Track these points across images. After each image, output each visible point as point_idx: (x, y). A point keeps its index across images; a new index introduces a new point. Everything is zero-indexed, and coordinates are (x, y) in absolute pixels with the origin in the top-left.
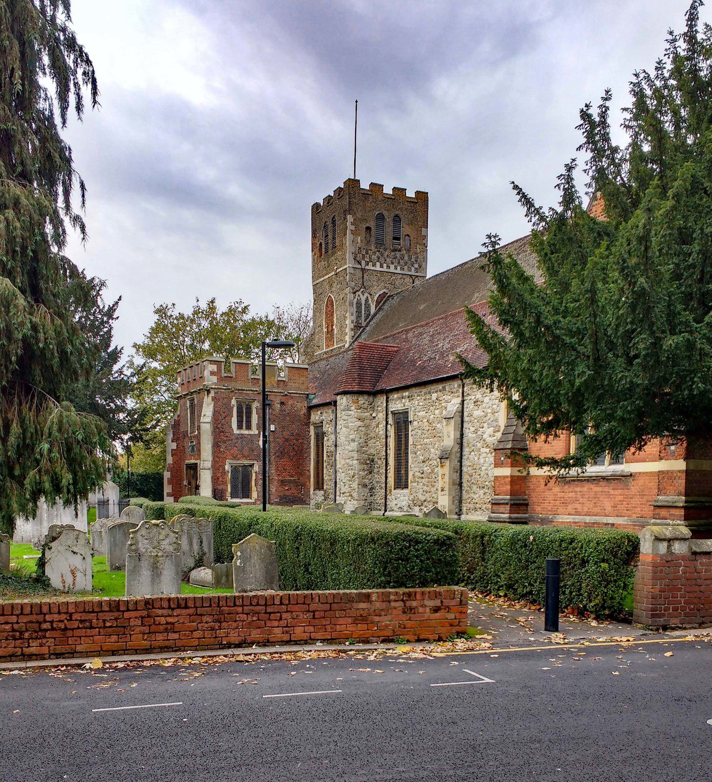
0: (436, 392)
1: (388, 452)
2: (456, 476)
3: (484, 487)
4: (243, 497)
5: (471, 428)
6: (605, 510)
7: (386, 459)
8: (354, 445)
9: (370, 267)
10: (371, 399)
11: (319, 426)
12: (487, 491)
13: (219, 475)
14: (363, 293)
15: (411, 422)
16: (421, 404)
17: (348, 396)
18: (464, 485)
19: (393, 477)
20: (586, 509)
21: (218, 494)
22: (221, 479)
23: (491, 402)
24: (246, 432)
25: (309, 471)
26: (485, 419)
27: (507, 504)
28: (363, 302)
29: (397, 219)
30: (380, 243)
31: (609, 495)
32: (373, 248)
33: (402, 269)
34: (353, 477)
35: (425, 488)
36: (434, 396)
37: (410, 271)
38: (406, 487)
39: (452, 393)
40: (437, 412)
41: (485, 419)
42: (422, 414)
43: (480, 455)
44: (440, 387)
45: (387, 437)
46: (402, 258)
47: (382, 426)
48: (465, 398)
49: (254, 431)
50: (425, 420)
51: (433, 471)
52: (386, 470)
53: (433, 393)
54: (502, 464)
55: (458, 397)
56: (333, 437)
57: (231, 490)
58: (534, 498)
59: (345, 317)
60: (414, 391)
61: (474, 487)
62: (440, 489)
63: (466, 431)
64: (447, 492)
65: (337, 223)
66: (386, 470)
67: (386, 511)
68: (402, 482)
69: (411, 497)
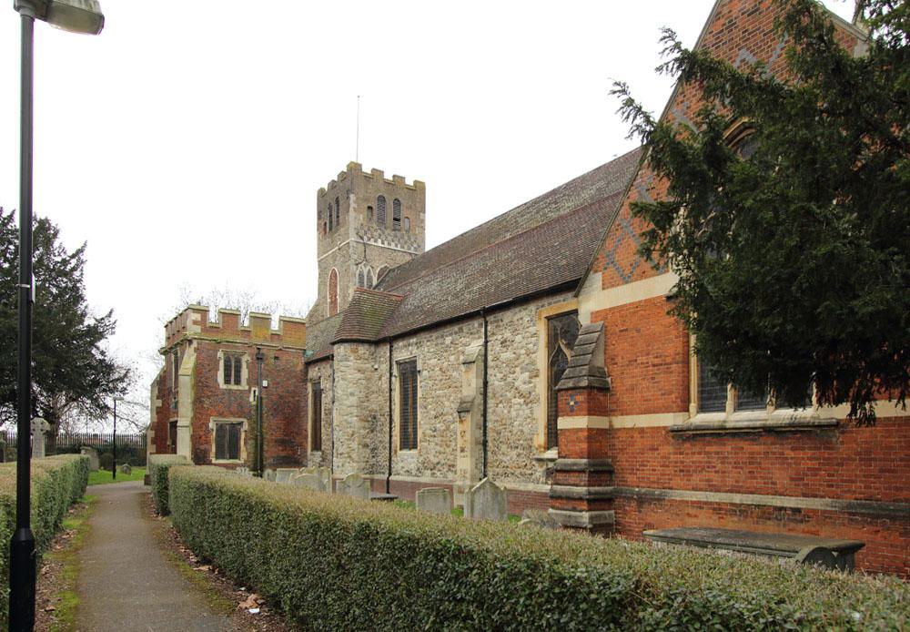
0: (451, 335)
1: (393, 407)
2: (479, 433)
3: (517, 448)
4: (230, 458)
5: (498, 374)
6: (774, 483)
7: (391, 416)
8: (354, 400)
9: (372, 242)
10: (373, 349)
11: (316, 383)
12: (521, 452)
13: (202, 433)
14: (365, 265)
15: (419, 372)
16: (432, 350)
17: (346, 345)
18: (490, 444)
19: (398, 434)
20: (730, 481)
21: (200, 458)
22: (203, 438)
23: (525, 341)
24: (235, 387)
25: (306, 430)
26: (516, 363)
27: (583, 471)
28: (365, 274)
29: (397, 203)
30: (381, 221)
31: (782, 459)
32: (375, 226)
33: (402, 247)
34: (353, 435)
35: (438, 448)
36: (448, 340)
37: (409, 249)
38: (415, 446)
39: (471, 334)
40: (452, 358)
41: (516, 363)
42: (434, 361)
43: (511, 407)
44: (456, 328)
45: (391, 390)
46: (402, 238)
47: (385, 378)
48: (489, 339)
49: (244, 386)
50: (437, 369)
51: (448, 428)
52: (391, 428)
53: (447, 336)
54: (572, 411)
55: (479, 338)
56: (331, 392)
57: (217, 450)
58: (623, 461)
59: (348, 287)
60: (424, 336)
61: (504, 448)
62: (459, 449)
63: (491, 379)
64: (468, 453)
65: (341, 202)
66: (391, 428)
67: (390, 474)
68: (409, 441)
69: (421, 459)
